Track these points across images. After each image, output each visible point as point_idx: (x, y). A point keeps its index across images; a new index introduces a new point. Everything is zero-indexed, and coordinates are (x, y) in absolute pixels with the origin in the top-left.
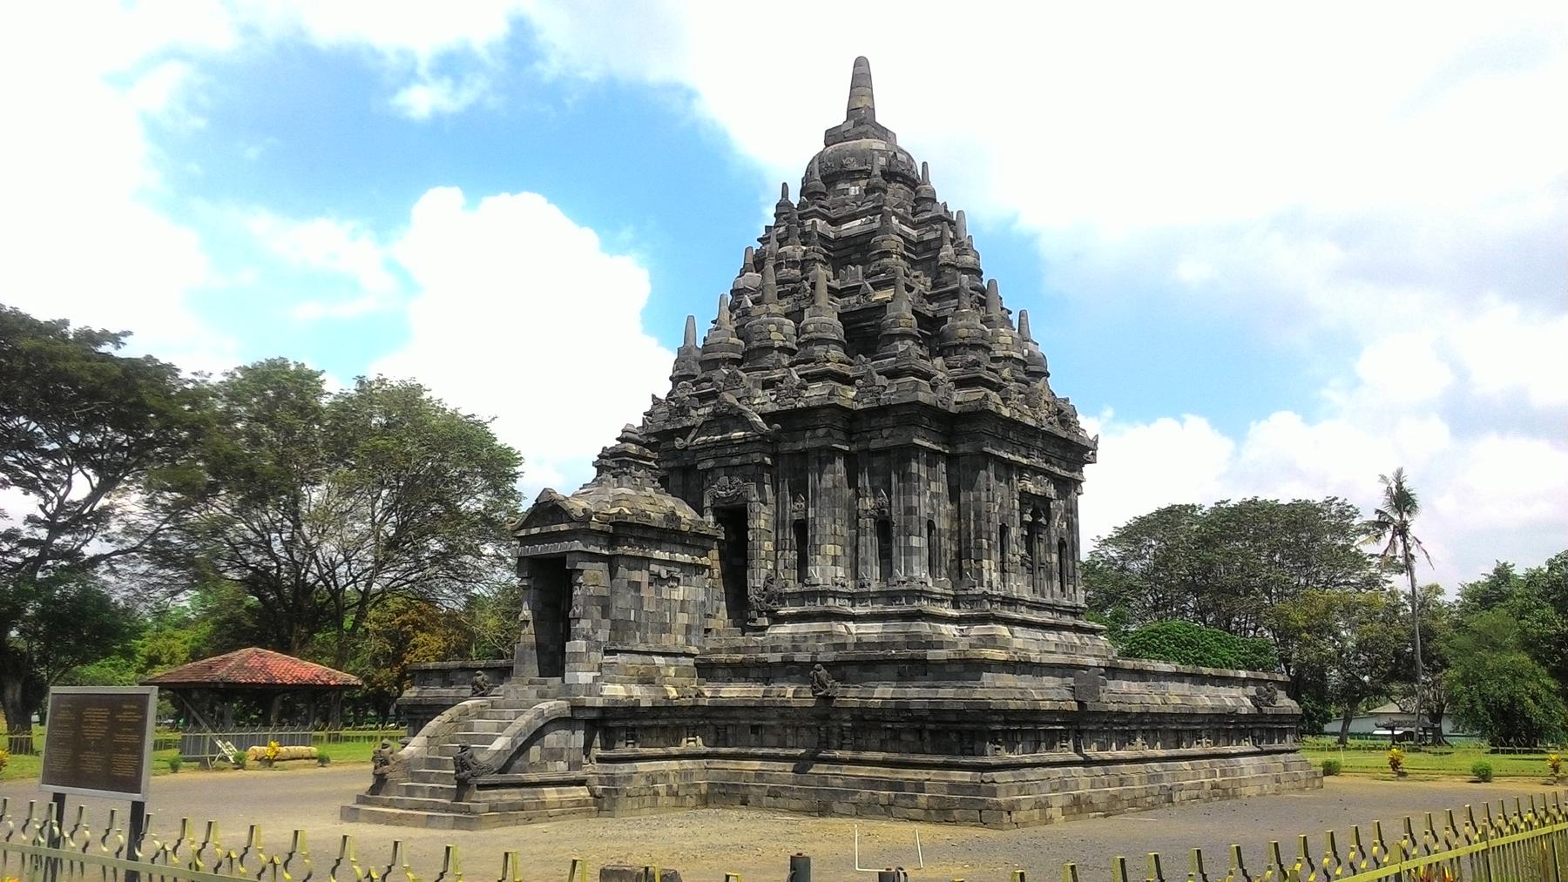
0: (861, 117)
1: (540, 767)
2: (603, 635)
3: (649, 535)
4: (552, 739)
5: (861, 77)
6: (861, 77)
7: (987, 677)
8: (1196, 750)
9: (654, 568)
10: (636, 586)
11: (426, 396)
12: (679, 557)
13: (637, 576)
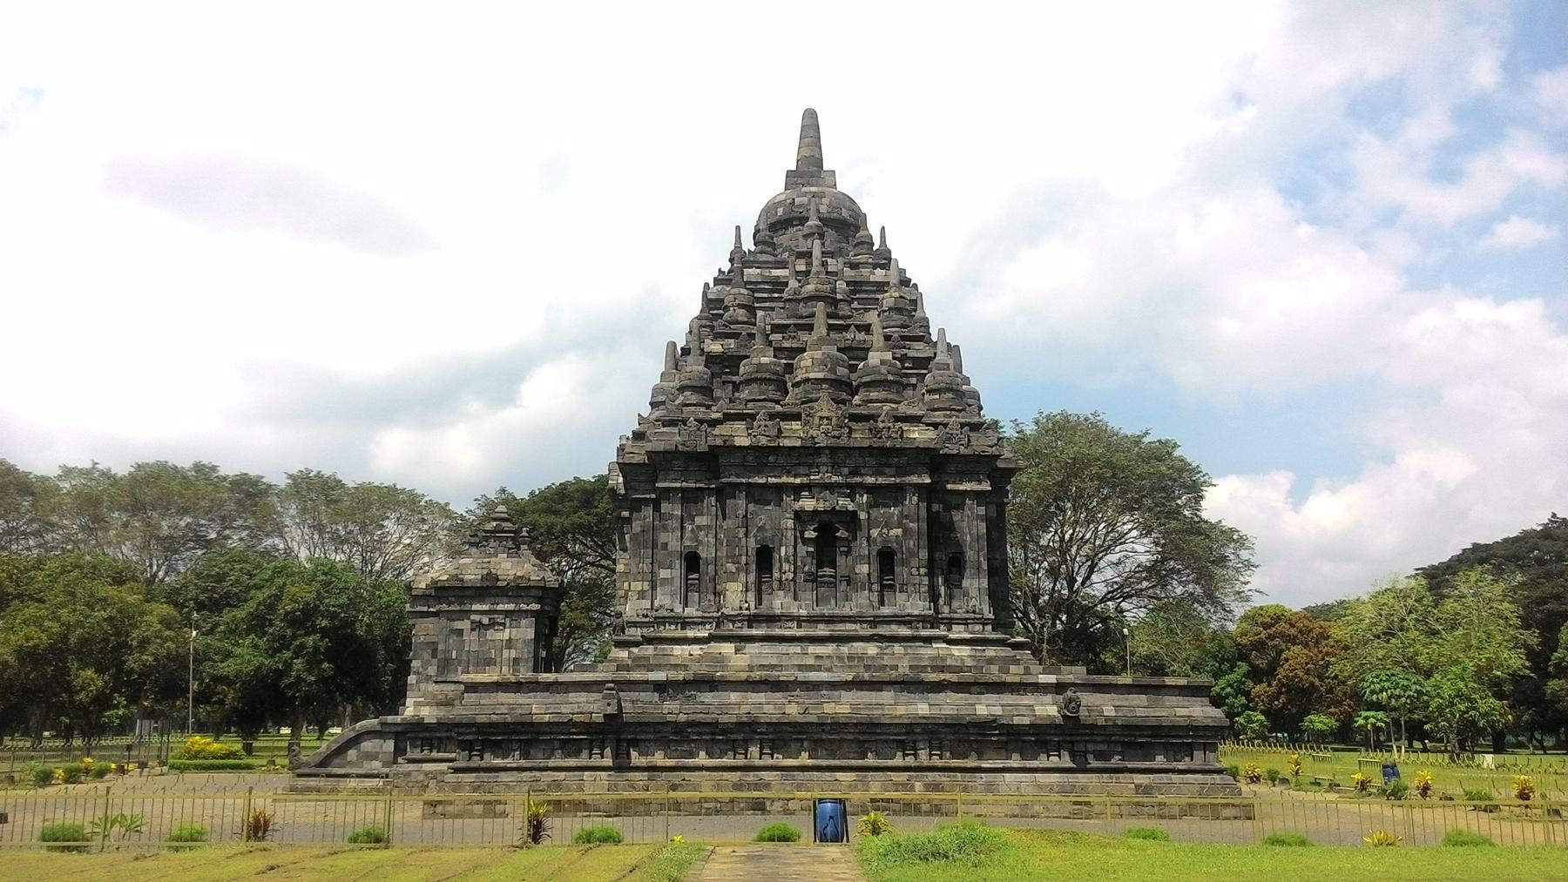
0: (809, 168)
1: (358, 764)
2: (432, 671)
3: (468, 593)
4: (367, 745)
5: (811, 126)
6: (811, 126)
7: (850, 678)
8: (508, 762)
9: (476, 617)
10: (460, 632)
11: (1176, 453)
12: (500, 607)
13: (458, 625)
